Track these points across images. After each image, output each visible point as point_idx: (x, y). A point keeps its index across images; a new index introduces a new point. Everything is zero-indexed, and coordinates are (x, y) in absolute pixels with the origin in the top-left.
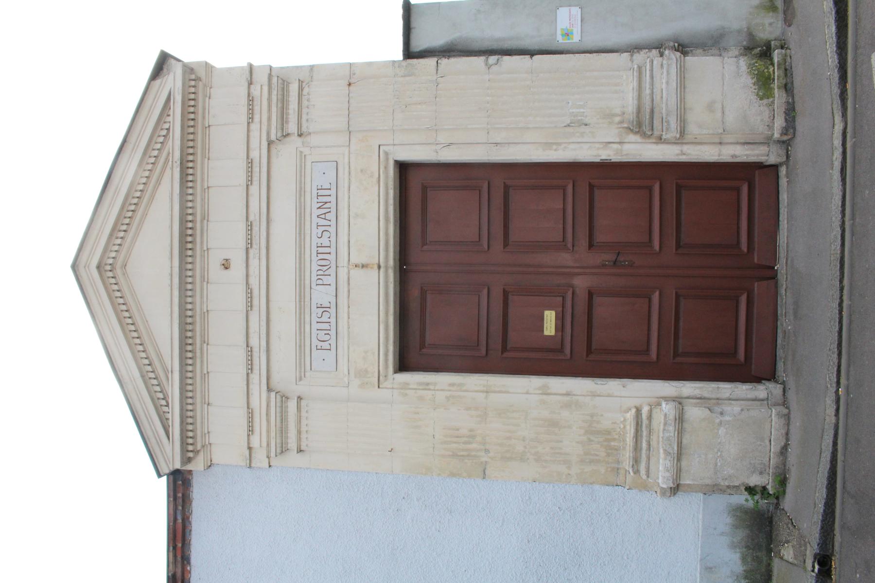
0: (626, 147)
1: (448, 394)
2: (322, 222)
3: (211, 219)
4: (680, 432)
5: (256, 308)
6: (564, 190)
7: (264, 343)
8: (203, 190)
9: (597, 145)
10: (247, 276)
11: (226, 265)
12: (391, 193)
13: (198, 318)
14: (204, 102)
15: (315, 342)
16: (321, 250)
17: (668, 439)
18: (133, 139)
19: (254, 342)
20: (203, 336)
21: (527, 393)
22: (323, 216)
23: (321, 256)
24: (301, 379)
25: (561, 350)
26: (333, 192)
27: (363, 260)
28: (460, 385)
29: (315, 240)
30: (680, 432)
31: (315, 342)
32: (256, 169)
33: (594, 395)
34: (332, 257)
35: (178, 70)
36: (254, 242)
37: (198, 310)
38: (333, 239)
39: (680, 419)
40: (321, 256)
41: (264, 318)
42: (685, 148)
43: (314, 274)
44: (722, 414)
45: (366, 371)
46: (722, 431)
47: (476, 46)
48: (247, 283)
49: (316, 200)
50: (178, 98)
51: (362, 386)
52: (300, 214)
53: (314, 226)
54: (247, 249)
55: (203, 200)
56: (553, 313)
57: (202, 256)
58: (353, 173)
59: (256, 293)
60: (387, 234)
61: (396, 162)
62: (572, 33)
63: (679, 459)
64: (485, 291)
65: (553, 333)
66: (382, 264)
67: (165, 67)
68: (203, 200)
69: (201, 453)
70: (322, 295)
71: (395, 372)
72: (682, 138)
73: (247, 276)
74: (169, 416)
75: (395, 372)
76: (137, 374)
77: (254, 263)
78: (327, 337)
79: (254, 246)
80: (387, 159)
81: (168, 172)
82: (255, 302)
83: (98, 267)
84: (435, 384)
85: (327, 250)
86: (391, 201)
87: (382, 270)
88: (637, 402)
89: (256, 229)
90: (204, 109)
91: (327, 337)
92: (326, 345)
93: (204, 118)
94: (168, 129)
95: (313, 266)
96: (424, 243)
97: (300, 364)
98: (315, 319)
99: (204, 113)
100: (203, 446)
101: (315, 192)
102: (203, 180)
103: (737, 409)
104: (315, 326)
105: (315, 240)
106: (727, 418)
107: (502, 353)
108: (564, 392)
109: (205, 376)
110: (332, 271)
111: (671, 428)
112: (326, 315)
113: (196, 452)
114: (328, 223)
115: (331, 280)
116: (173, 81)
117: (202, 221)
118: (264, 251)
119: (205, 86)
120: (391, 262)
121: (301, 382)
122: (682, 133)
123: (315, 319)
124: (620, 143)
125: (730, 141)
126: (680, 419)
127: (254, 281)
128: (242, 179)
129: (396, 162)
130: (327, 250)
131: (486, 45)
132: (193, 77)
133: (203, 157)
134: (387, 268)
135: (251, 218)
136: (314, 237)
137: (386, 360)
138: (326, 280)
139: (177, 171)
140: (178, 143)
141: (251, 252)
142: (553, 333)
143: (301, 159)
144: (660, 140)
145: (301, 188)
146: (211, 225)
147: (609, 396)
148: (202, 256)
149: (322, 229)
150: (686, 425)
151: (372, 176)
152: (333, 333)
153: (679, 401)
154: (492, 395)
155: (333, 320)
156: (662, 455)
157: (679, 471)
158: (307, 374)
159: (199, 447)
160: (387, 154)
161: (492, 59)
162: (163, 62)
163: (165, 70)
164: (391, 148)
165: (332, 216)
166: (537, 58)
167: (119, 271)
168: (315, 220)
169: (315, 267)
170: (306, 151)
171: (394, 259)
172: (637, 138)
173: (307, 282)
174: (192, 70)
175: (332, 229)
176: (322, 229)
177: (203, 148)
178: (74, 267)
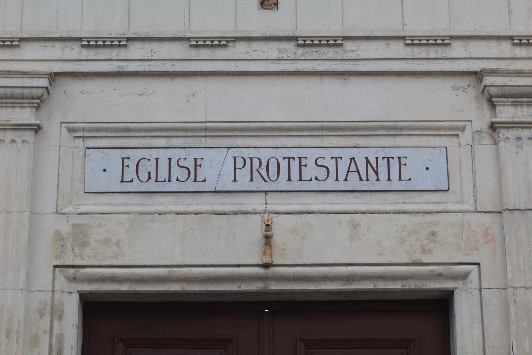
5: (194, 53)
7: (133, 67)
10: (250, 39)
19: (136, 51)
22: (353, 168)
24: (71, 130)
26: (396, 185)
32: (432, 52)
34: (283, 184)
36: (307, 50)
38: (314, 186)
40: (284, 165)
43: (253, 153)
45: (84, 245)
48: (237, 39)
49: (381, 154)
51: (58, 237)
53: (336, 153)
54: (404, 38)
58: (428, 218)
60: (324, 278)
70: (217, 166)
71: (83, 296)
73: (250, 39)
75: (83, 296)
77: (272, 50)
78: (144, 176)
79: (301, 51)
80: (455, 277)
82: (205, 53)
85: (295, 175)
86: (381, 286)
89: (330, 53)
92: (130, 174)
98: (176, 154)
101: (395, 153)
104: (163, 155)
110: (258, 184)
112: (182, 174)
114: (341, 177)
115: (243, 183)
120: (274, 287)
121: (65, 131)
123: (176, 154)
127: (240, 50)
128: (415, 29)
130: (295, 175)
135: (349, 45)
136: (316, 153)
138: (243, 174)
141: (290, 46)
151: (424, 251)
152: (152, 186)
155: (174, 186)
160: (464, 277)
165: (354, 183)
169: (265, 155)
170: (466, 137)
173: (239, 142)
175: (330, 184)
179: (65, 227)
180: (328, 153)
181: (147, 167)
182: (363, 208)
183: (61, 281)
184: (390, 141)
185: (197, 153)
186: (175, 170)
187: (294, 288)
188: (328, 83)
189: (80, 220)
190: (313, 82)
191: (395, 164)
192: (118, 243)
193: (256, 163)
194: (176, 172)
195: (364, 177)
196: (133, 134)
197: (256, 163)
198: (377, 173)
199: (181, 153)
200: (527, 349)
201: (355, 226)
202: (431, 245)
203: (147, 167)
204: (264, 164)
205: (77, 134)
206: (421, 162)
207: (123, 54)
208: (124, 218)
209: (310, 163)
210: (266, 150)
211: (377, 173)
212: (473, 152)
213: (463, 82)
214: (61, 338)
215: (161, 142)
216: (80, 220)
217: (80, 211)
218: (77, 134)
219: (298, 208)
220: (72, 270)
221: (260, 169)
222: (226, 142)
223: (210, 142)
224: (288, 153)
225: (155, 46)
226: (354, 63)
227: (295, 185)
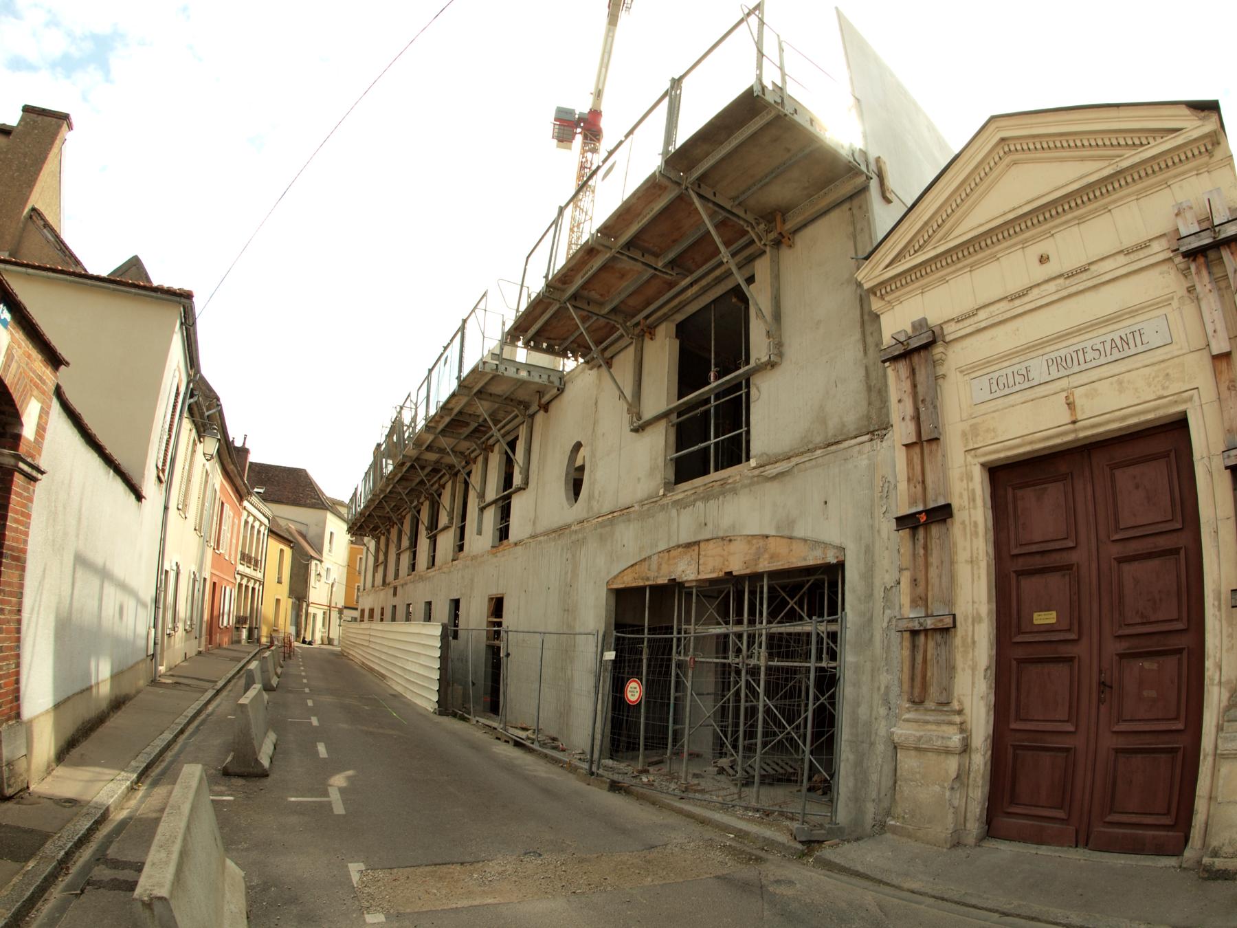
0: (1215, 689)
1: (967, 522)
3: (1082, 226)
4: (938, 751)
5: (1011, 304)
6: (1176, 620)
7: (983, 325)
8: (1105, 207)
9: (1218, 655)
10: (1038, 285)
11: (1043, 259)
12: (1151, 416)
13: (988, 252)
14: (1191, 170)
15: (995, 375)
16: (1080, 353)
17: (931, 739)
18: (1123, 113)
19: (982, 315)
20: (927, 285)
21: (973, 602)
25: (1020, 632)
26: (1141, 348)
27: (1078, 402)
28: (976, 533)
29: (1088, 344)
30: (938, 751)
31: (995, 375)
32: (1141, 254)
33: (974, 669)
34: (1076, 369)
35: (1210, 126)
37: (997, 248)
38: (1094, 364)
39: (948, 752)
41: (1006, 316)
42: (1210, 759)
44: (953, 788)
45: (977, 435)
46: (937, 788)
48: (1031, 288)
49: (1128, 331)
50: (1180, 140)
51: (964, 434)
54: (1122, 251)
55: (1096, 210)
56: (1054, 621)
57: (1044, 232)
58: (1163, 365)
59: (1026, 299)
60: (1108, 422)
61: (1185, 413)
63: (917, 749)
65: (1035, 622)
67: (1206, 113)
68: (1096, 210)
69: (883, 303)
70: (1039, 369)
71: (983, 465)
72: (1218, 756)
73: (1038, 285)
74: (908, 258)
75: (983, 465)
76: (925, 218)
77: (1051, 287)
78: (1001, 386)
79: (1068, 282)
80: (1185, 401)
81: (1105, 163)
82: (1017, 302)
83: (1003, 140)
84: (975, 508)
85: (1082, 360)
86: (1143, 418)
87: (1071, 427)
88: (967, 711)
89: (1084, 276)
90: (1121, 198)
91: (1001, 386)
92: (994, 387)
93: (1175, 177)
94: (1142, 145)
95: (1062, 350)
98: (1015, 369)
99: (1179, 175)
101: (1136, 328)
102: (1115, 201)
103: (956, 803)
104: (1009, 371)
105: (1088, 344)
106: (948, 794)
107: (1015, 572)
108: (976, 638)
109: (944, 280)
110: (1063, 373)
111: (939, 743)
112: (1018, 379)
113: (882, 297)
115: (1055, 374)
116: (1196, 127)
117: (1075, 218)
118: (1064, 293)
119: (1207, 164)
120: (1082, 435)
122: (1224, 757)
123: (1015, 369)
124: (1220, 683)
125: (76, 592)
126: (948, 752)
127: (1035, 293)
128: (1128, 242)
130: (1082, 360)
132: (1209, 147)
133: (1138, 192)
134: (1075, 431)
135: (1093, 268)
136: (1091, 343)
138: (1053, 369)
139: (1106, 173)
140: (1137, 159)
141: (1061, 281)
142: (1035, 622)
144: (1220, 728)
146: (1076, 229)
147: (973, 683)
148: (1044, 232)
149: (1100, 347)
150: (943, 756)
151: (1164, 388)
152: (1007, 391)
153: (966, 748)
154: (969, 567)
155: (1018, 388)
156: (918, 734)
157: (907, 748)
158: (967, 378)
159: (887, 299)
160: (1191, 399)
162: (1210, 108)
163: (1203, 114)
164: (1197, 403)
165: (1116, 355)
167: (1007, 160)
168: (1108, 338)
169: (1063, 353)
170: (1175, 303)
171: (1086, 438)
172: (1224, 703)
173: (1048, 349)
174: (1216, 143)
175: (1103, 360)
176: (1100, 347)
177: (1145, 189)
178: (993, 118)
179: (965, 426)
180: (1098, 341)
181: (1002, 380)
182: (1123, 370)
183: (969, 458)
184: (1132, 321)
185: (1026, 364)
186: (1017, 378)
188: (1090, 296)
189: (974, 421)
190: (1080, 298)
191: (1137, 334)
194: (1018, 379)
199: (1018, 366)
200: (231, 798)
201: (1120, 383)
203: (1002, 380)
206: (1152, 328)
207: (976, 319)
210: (1062, 350)
212: (1181, 313)
213: (1164, 268)
214: (973, 490)
215: (1017, 360)
216: (974, 421)
222: (1041, 352)
223: (1033, 355)
224: (1075, 348)
225: (992, 308)
227: (1084, 367)
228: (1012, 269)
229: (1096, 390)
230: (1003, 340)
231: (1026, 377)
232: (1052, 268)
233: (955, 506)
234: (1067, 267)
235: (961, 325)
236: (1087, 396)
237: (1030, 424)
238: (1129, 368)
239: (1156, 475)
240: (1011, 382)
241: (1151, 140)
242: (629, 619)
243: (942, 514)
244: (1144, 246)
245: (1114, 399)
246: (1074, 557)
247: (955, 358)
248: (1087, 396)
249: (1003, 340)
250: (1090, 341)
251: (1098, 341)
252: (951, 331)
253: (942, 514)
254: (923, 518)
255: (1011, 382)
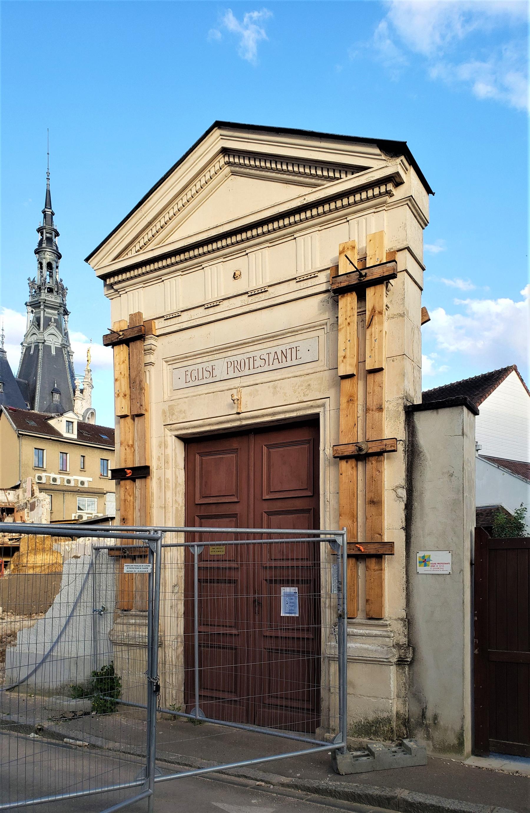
2: (272, 357)
10: (229, 298)
22: (276, 357)
23: (247, 361)
24: (166, 362)
26: (295, 362)
32: (309, 283)
34: (247, 372)
36: (253, 297)
40: (247, 361)
43: (234, 358)
47: (417, 475)
52: (278, 336)
53: (268, 351)
59: (217, 309)
60: (263, 416)
61: (318, 415)
62: (425, 566)
64: (236, 500)
66: (242, 415)
69: (112, 291)
70: (221, 369)
73: (229, 298)
78: (193, 379)
80: (319, 406)
82: (211, 310)
86: (294, 414)
89: (263, 296)
92: (189, 378)
96: (269, 447)
97: (175, 360)
98: (204, 365)
100: (116, 290)
101: (294, 345)
104: (200, 367)
107: (197, 516)
112: (206, 374)
114: (271, 364)
115: (231, 375)
117: (267, 241)
120: (245, 422)
121: (164, 362)
123: (204, 365)
127: (225, 305)
129: (318, 415)
131: (417, 485)
134: (240, 419)
136: (260, 353)
137: (181, 429)
138: (231, 369)
143: (320, 325)
145: (297, 331)
161: (403, 493)
165: (277, 365)
166: (403, 534)
169: (239, 358)
173: (229, 354)
175: (266, 368)
180: (265, 352)
185: (212, 363)
187: (386, 483)
191: (294, 350)
192: (184, 412)
193: (236, 362)
195: (280, 362)
196: (189, 359)
197: (236, 362)
198: (286, 358)
202: (308, 391)
203: (195, 373)
204: (239, 363)
205: (169, 363)
208: (186, 400)
209: (258, 358)
210: (239, 355)
211: (286, 358)
217: (171, 399)
218: (169, 363)
219: (252, 383)
220: (169, 426)
221: (237, 366)
222: (224, 355)
224: (248, 355)
226: (274, 299)
228: (214, 278)
229: (257, 391)
230: (198, 340)
231: (211, 373)
232: (241, 286)
233: (154, 465)
234: (253, 286)
235: (169, 322)
236: (250, 394)
237: (210, 411)
238: (283, 377)
239: (297, 454)
240: (201, 377)
241: (343, 176)
242: (373, 509)
243: (142, 472)
244: (313, 276)
245: (268, 399)
246: (237, 509)
247: (160, 348)
248: (250, 394)
249: (198, 340)
250: (259, 351)
251: (265, 352)
252: (159, 327)
253: (142, 472)
254: (129, 473)
255: (201, 377)
